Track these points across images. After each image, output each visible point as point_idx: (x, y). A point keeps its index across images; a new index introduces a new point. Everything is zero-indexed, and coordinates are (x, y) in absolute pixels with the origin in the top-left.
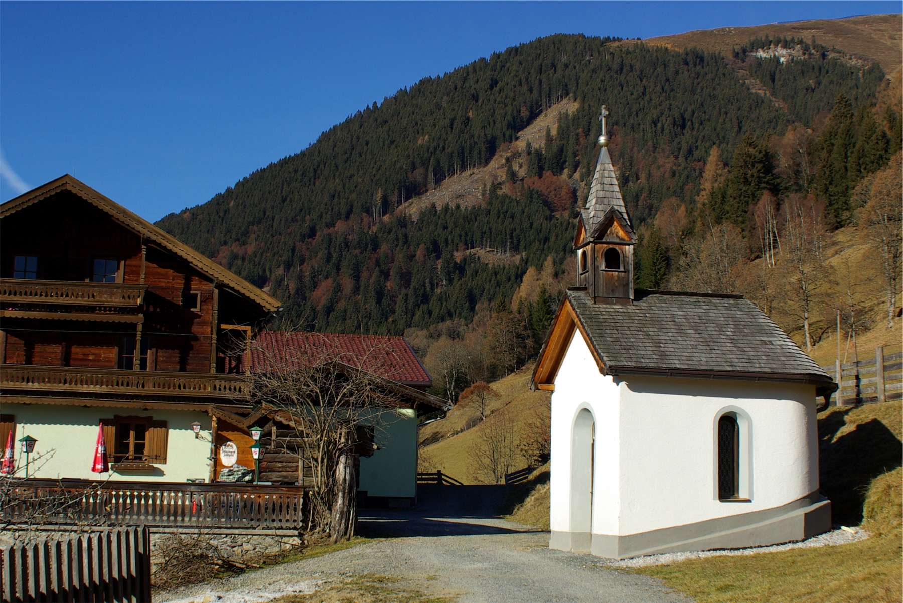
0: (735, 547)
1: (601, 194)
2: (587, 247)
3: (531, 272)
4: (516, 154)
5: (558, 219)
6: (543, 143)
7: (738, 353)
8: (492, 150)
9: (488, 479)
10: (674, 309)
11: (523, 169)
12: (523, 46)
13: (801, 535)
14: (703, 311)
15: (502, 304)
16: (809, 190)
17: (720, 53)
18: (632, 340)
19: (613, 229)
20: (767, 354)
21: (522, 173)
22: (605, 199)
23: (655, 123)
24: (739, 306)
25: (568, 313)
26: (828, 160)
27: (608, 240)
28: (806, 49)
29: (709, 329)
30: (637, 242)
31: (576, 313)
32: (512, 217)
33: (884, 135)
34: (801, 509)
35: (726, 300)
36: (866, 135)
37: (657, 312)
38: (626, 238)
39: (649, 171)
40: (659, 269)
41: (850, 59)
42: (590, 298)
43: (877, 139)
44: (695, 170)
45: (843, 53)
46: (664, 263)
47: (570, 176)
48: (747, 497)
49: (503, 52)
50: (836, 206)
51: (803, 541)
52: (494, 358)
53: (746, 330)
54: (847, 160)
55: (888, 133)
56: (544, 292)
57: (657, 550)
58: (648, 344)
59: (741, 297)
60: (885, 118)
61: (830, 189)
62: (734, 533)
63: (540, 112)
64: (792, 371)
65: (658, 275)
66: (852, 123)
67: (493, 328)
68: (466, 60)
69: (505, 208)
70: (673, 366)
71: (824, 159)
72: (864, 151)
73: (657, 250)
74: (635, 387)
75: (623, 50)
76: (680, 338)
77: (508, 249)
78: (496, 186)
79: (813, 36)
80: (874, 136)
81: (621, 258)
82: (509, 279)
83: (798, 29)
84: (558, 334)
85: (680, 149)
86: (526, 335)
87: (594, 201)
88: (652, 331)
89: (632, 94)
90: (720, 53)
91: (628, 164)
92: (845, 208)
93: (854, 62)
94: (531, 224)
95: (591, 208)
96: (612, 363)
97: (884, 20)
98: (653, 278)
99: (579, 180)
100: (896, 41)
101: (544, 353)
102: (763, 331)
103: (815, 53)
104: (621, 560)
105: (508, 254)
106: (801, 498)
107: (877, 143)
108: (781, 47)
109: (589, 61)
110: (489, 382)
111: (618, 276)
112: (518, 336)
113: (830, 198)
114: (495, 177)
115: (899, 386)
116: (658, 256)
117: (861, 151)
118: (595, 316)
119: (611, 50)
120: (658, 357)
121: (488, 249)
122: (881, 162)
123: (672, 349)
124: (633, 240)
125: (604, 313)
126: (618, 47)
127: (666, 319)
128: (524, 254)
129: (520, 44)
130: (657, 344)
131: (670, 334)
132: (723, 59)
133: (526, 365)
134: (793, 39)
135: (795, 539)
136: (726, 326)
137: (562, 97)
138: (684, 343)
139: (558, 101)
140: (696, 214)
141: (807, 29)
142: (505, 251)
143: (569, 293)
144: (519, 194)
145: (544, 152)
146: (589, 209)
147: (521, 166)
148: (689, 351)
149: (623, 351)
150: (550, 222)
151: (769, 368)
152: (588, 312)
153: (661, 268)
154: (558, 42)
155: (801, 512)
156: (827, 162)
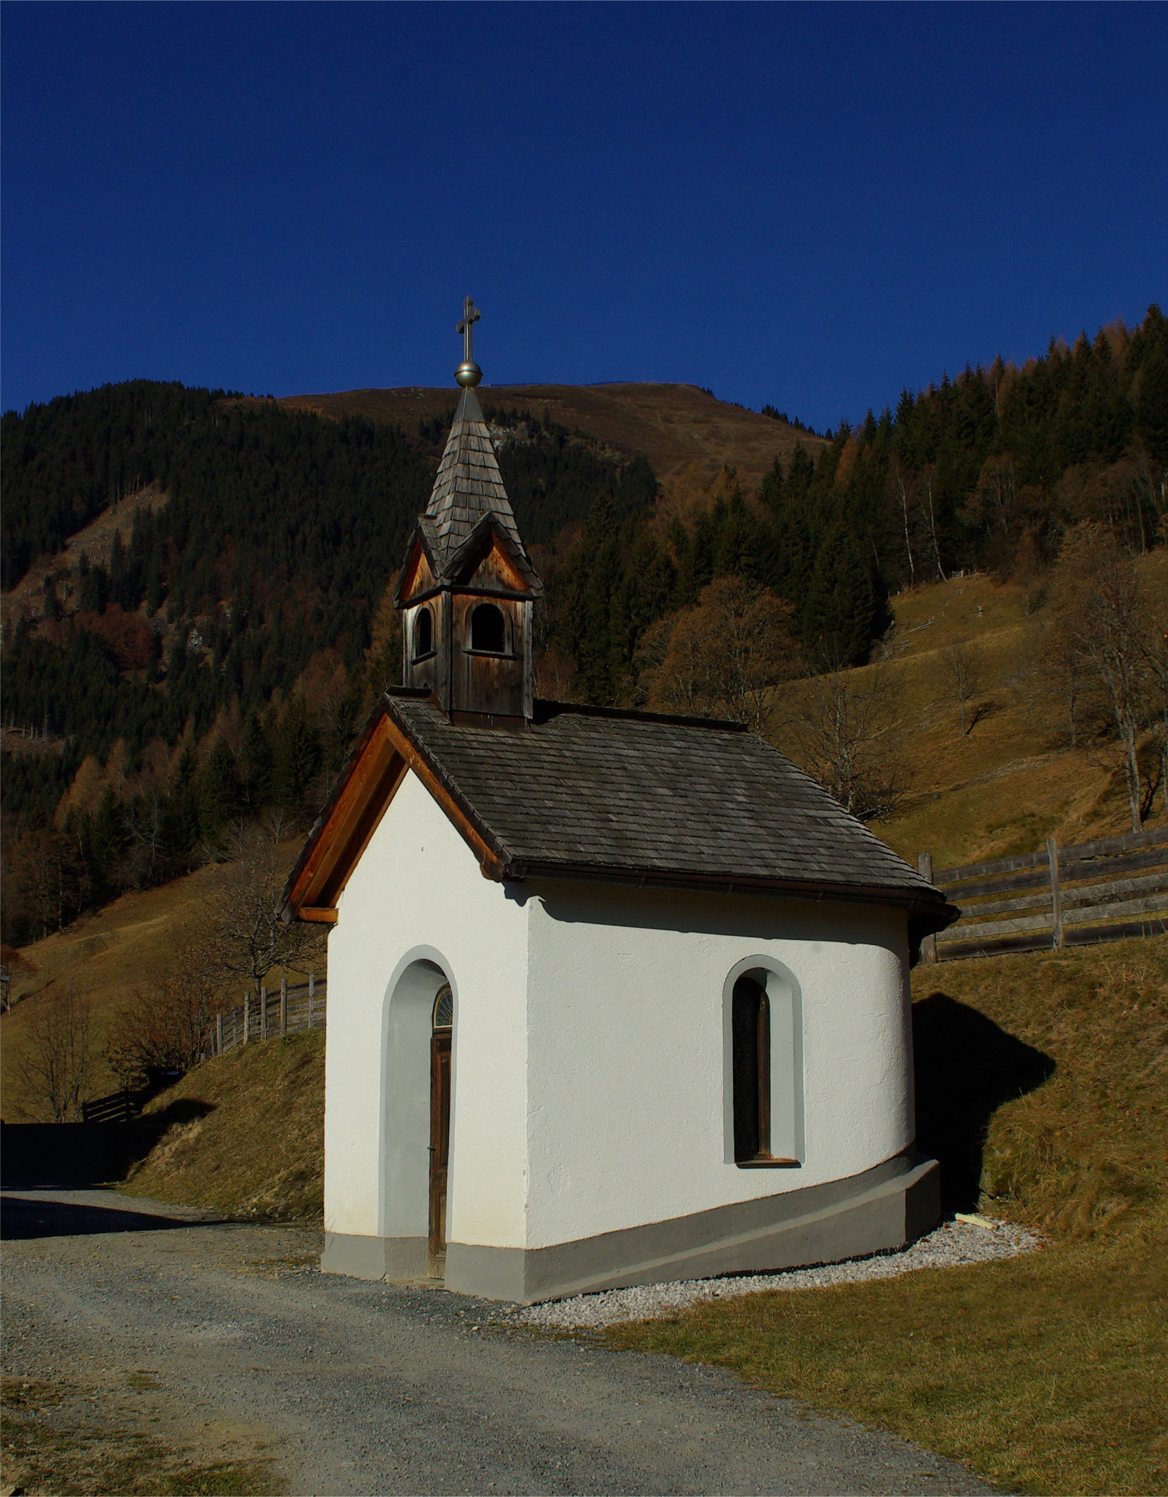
0: (771, 1267)
1: (464, 485)
2: (432, 601)
3: (88, 765)
4: (64, 574)
5: (129, 683)
6: (108, 558)
7: (770, 839)
8: (22, 566)
9: (40, 1113)
10: (618, 744)
11: (74, 598)
12: (80, 396)
13: (898, 1233)
14: (675, 750)
15: (39, 816)
16: (547, 646)
17: (399, 427)
18: (549, 804)
19: (491, 564)
20: (829, 844)
21: (72, 604)
22: (472, 498)
23: (292, 533)
24: (744, 745)
26: (578, 598)
27: (480, 586)
28: (534, 429)
29: (698, 787)
30: (541, 593)
31: (415, 743)
32: (54, 676)
33: (668, 563)
34: (895, 1179)
35: (713, 733)
36: (640, 561)
37: (584, 748)
38: (517, 584)
39: (281, 610)
40: (303, 767)
41: (603, 449)
42: (438, 713)
43: (658, 569)
44: (354, 612)
45: (592, 439)
46: (312, 756)
47: (152, 614)
48: (791, 1156)
49: (47, 403)
50: (589, 673)
51: (904, 1249)
52: (25, 907)
53: (771, 795)
54: (609, 600)
55: (674, 560)
56: (111, 797)
57: (612, 1280)
58: (584, 815)
59: (744, 728)
60: (670, 537)
61: (582, 646)
62: (768, 1237)
63: (104, 508)
64: (887, 881)
65: (300, 775)
66: (617, 541)
67: (24, 856)
69: (42, 660)
70: (648, 863)
71: (574, 598)
72: (636, 586)
73: (300, 734)
74: (561, 909)
75: (244, 413)
76: (645, 804)
77: (45, 729)
78: (28, 624)
79: (547, 409)
80: (653, 564)
81: (507, 629)
82: (46, 779)
83: (523, 396)
84: (357, 794)
85: (331, 577)
86: (79, 868)
87: (448, 501)
88: (585, 787)
89: (256, 485)
90: (399, 427)
91: (246, 598)
92: (603, 676)
93: (608, 453)
94: (85, 690)
95: (441, 517)
96: (520, 852)
97: (657, 391)
98: (292, 779)
99: (166, 620)
100: (671, 426)
101: (319, 837)
102: (805, 798)
103: (548, 436)
104: (534, 1305)
105: (45, 738)
106: (895, 1157)
107: (658, 575)
108: (496, 423)
109: (189, 427)
110: (19, 947)
111: (500, 665)
112: (66, 870)
113: (580, 660)
114: (27, 610)
115: (968, 931)
116: (301, 743)
117: (632, 586)
118: (456, 750)
119: (224, 412)
120: (609, 842)
121: (12, 728)
122: (662, 606)
123: (635, 827)
124: (533, 591)
125: (475, 744)
126: (236, 407)
127: (607, 765)
128: (71, 738)
129: (76, 393)
130: (603, 814)
131: (622, 795)
132: (404, 436)
133: (79, 919)
134: (515, 412)
135: (888, 1246)
136: (728, 783)
137: (141, 483)
138: (655, 814)
139: (136, 491)
140: (364, 678)
141: (537, 397)
142: (41, 733)
143: (392, 700)
144: (66, 639)
145: (109, 572)
146: (434, 517)
147: (70, 593)
148: (671, 831)
149: (537, 827)
150: (117, 686)
151: (842, 873)
152: (441, 742)
153: (306, 763)
154: (138, 393)
155: (897, 1187)
156: (577, 602)
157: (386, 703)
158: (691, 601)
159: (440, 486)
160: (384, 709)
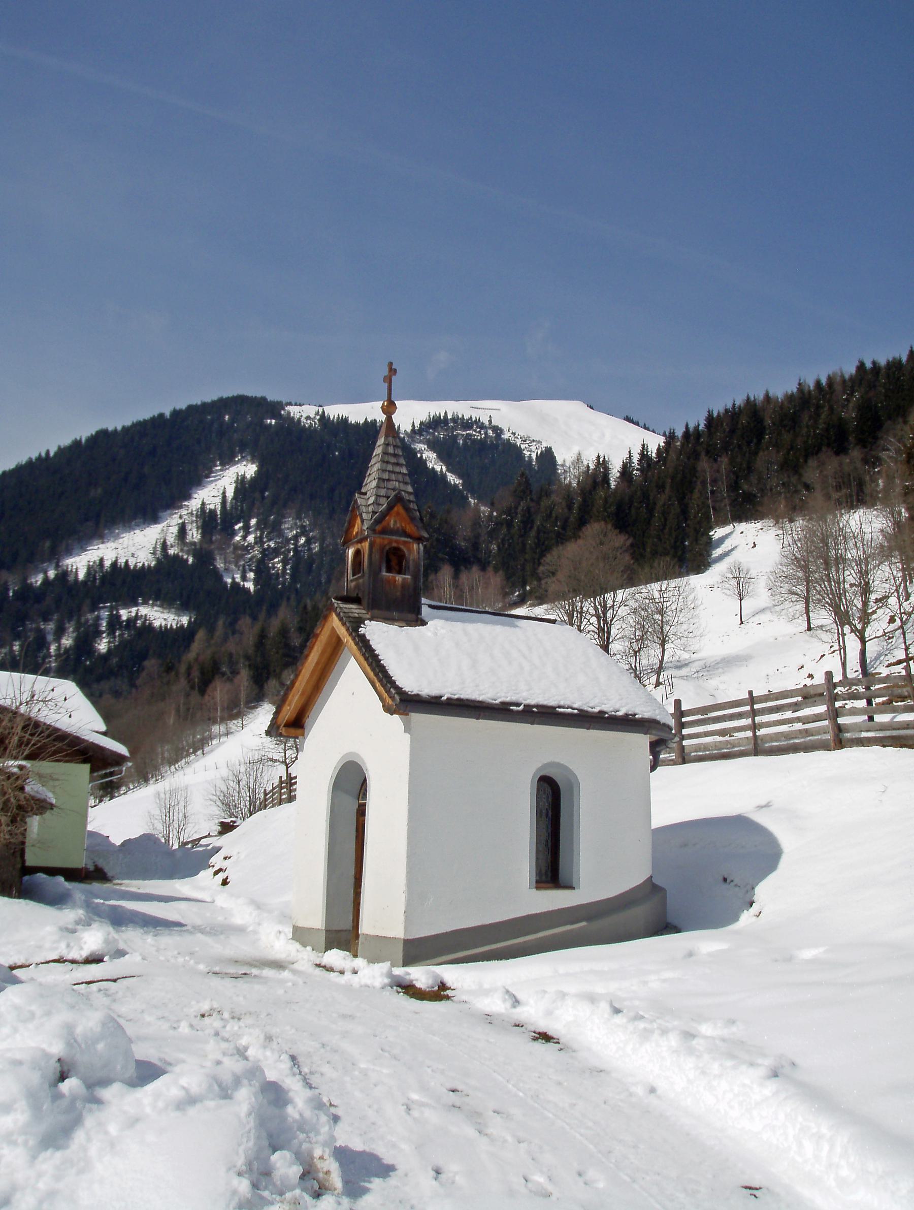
25: (333, 630)
68: (145, 414)
87: (374, 484)
157: (332, 604)
158: (576, 537)
159: (370, 474)
160: (331, 608)
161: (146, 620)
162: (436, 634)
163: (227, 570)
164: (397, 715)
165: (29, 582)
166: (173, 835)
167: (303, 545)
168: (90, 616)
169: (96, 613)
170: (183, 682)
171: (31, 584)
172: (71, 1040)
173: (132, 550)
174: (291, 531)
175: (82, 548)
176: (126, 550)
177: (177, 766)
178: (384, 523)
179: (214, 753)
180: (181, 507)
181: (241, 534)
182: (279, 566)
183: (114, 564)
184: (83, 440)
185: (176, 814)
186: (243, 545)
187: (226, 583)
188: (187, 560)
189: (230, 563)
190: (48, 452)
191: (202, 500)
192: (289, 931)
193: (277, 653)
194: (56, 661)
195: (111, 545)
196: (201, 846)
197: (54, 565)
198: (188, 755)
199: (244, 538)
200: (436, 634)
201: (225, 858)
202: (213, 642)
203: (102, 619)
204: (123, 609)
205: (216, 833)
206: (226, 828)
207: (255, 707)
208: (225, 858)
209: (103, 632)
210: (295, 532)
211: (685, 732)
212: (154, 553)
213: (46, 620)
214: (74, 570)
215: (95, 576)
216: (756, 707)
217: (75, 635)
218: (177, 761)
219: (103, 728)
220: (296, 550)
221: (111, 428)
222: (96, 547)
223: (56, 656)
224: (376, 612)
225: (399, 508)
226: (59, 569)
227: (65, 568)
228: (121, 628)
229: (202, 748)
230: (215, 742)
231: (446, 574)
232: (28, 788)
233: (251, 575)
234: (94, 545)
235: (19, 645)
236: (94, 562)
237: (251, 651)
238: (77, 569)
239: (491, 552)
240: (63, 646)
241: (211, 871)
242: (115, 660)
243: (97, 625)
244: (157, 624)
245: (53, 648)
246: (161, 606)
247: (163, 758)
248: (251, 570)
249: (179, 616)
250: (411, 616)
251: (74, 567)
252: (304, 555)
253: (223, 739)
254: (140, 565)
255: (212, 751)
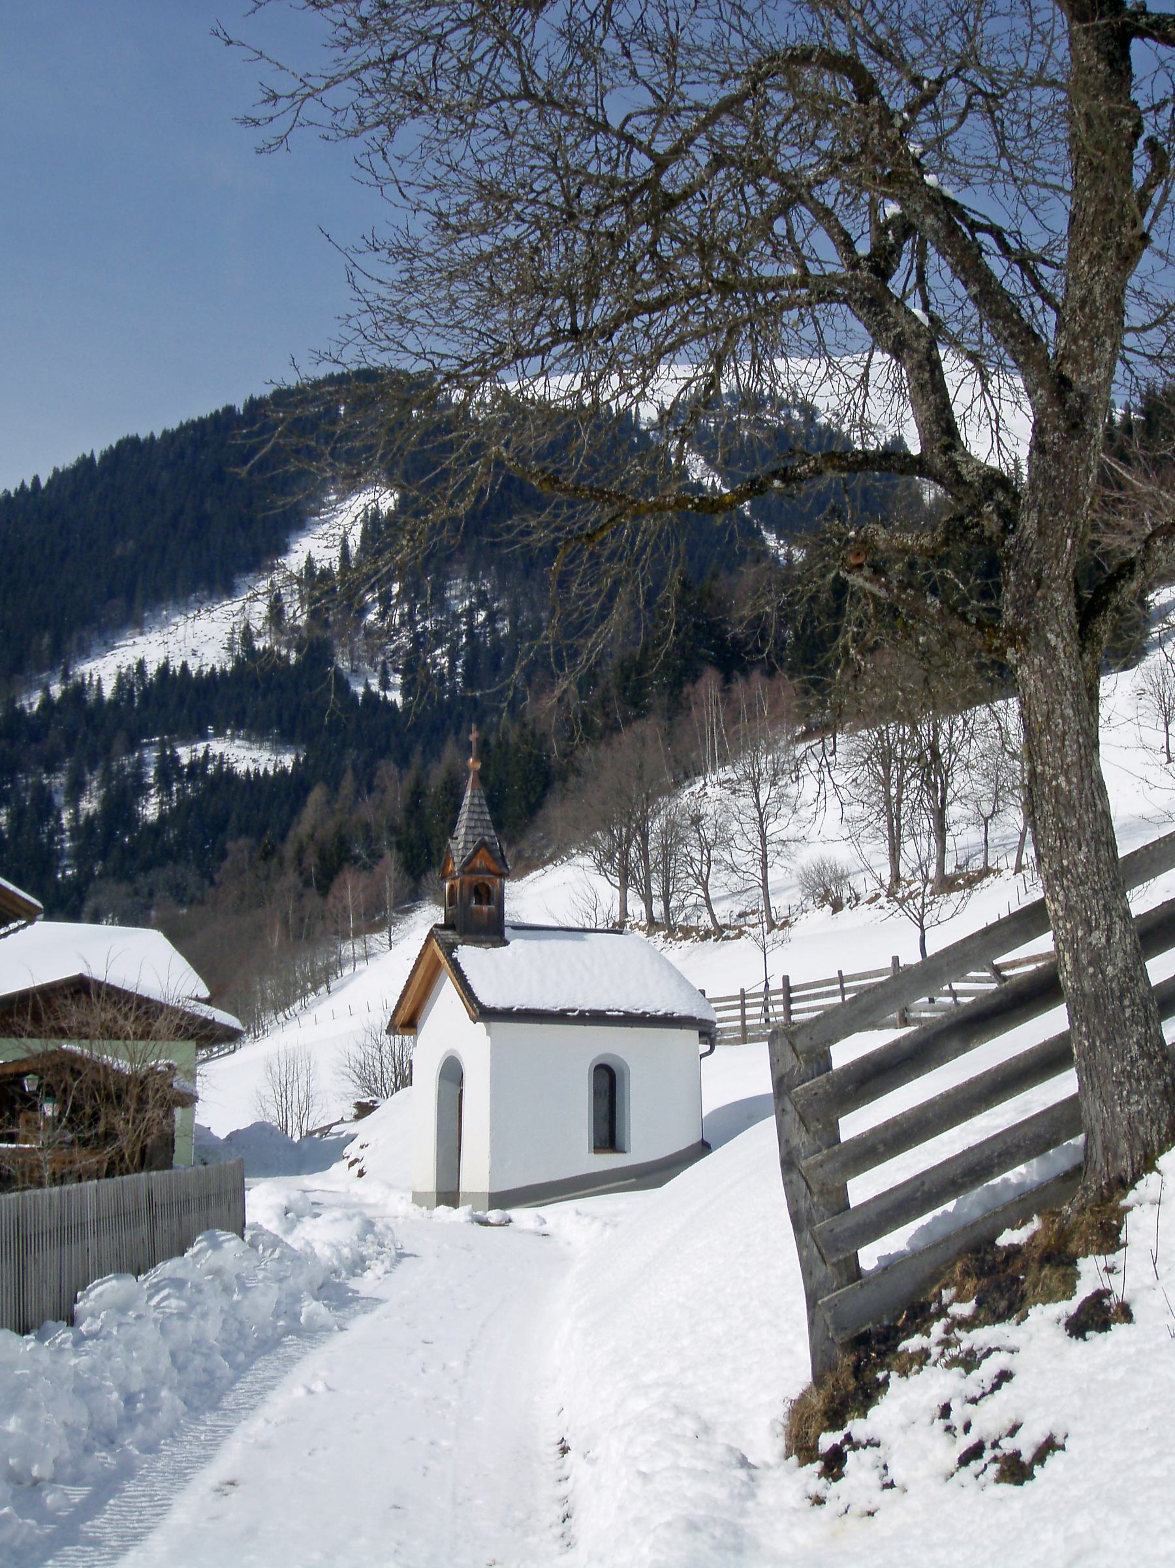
87: (463, 831)
161: (222, 763)
162: (515, 953)
163: (355, 671)
164: (482, 1024)
165: (18, 705)
166: (293, 1123)
167: (482, 625)
168: (125, 760)
169: (137, 754)
170: (291, 878)
171: (22, 709)
172: (290, 1201)
173: (193, 644)
174: (462, 602)
175: (106, 643)
176: (182, 644)
177: (287, 1012)
178: (472, 864)
179: (345, 990)
180: (272, 569)
181: (376, 610)
182: (444, 661)
183: (164, 670)
184: (97, 458)
185: (295, 1093)
186: (381, 628)
187: (355, 695)
188: (287, 657)
189: (360, 659)
190: (36, 480)
191: (306, 554)
192: (410, 1196)
193: (443, 821)
194: (72, 838)
195: (155, 637)
196: (332, 1134)
197: (59, 675)
198: (305, 994)
199: (382, 616)
200: (515, 953)
201: (362, 1147)
202: (337, 806)
203: (148, 765)
204: (182, 745)
205: (352, 1117)
206: (364, 1110)
207: (410, 911)
208: (362, 1147)
209: (151, 786)
210: (467, 603)
211: (793, 1007)
212: (230, 649)
213: (51, 770)
214: (95, 683)
215: (131, 692)
216: (845, 985)
217: (102, 792)
218: (288, 1005)
219: (205, 993)
220: (470, 633)
221: (144, 434)
222: (130, 642)
223: (71, 829)
224: (467, 936)
225: (483, 851)
226: (70, 682)
227: (79, 680)
228: (180, 778)
229: (327, 982)
230: (347, 971)
231: (709, 684)
232: (175, 1085)
233: (397, 679)
234: (127, 639)
235: (7, 814)
236: (129, 668)
237: (399, 819)
238: (99, 681)
239: (784, 642)
240: (83, 814)
241: (346, 1162)
242: (172, 833)
243: (139, 776)
244: (241, 769)
245: (66, 817)
246: (247, 738)
247: (264, 1000)
248: (396, 671)
249: (278, 753)
250: (496, 938)
251: (95, 678)
252: (485, 642)
253: (360, 966)
254: (208, 669)
255: (342, 987)
